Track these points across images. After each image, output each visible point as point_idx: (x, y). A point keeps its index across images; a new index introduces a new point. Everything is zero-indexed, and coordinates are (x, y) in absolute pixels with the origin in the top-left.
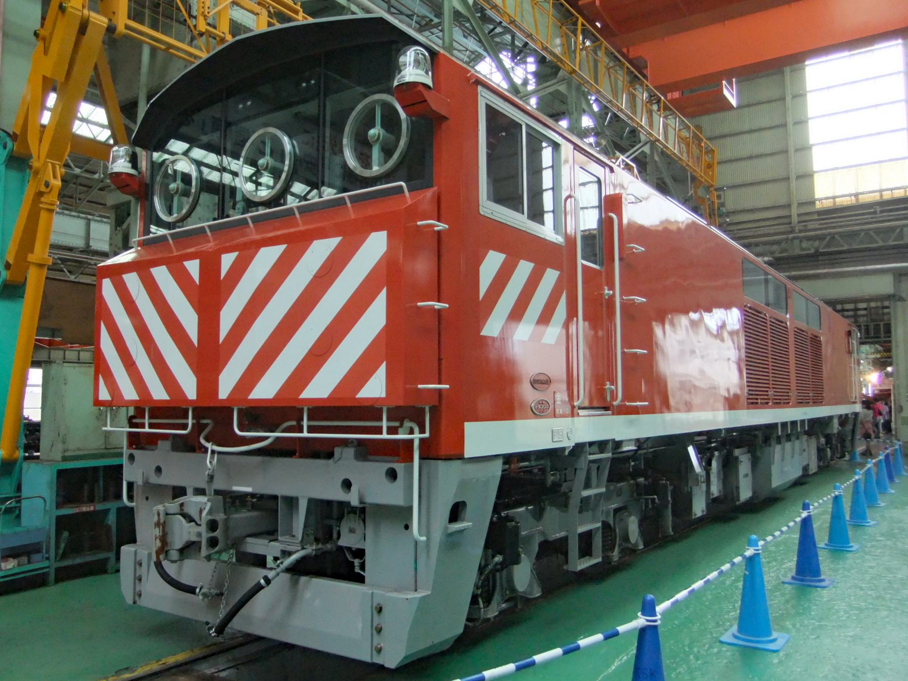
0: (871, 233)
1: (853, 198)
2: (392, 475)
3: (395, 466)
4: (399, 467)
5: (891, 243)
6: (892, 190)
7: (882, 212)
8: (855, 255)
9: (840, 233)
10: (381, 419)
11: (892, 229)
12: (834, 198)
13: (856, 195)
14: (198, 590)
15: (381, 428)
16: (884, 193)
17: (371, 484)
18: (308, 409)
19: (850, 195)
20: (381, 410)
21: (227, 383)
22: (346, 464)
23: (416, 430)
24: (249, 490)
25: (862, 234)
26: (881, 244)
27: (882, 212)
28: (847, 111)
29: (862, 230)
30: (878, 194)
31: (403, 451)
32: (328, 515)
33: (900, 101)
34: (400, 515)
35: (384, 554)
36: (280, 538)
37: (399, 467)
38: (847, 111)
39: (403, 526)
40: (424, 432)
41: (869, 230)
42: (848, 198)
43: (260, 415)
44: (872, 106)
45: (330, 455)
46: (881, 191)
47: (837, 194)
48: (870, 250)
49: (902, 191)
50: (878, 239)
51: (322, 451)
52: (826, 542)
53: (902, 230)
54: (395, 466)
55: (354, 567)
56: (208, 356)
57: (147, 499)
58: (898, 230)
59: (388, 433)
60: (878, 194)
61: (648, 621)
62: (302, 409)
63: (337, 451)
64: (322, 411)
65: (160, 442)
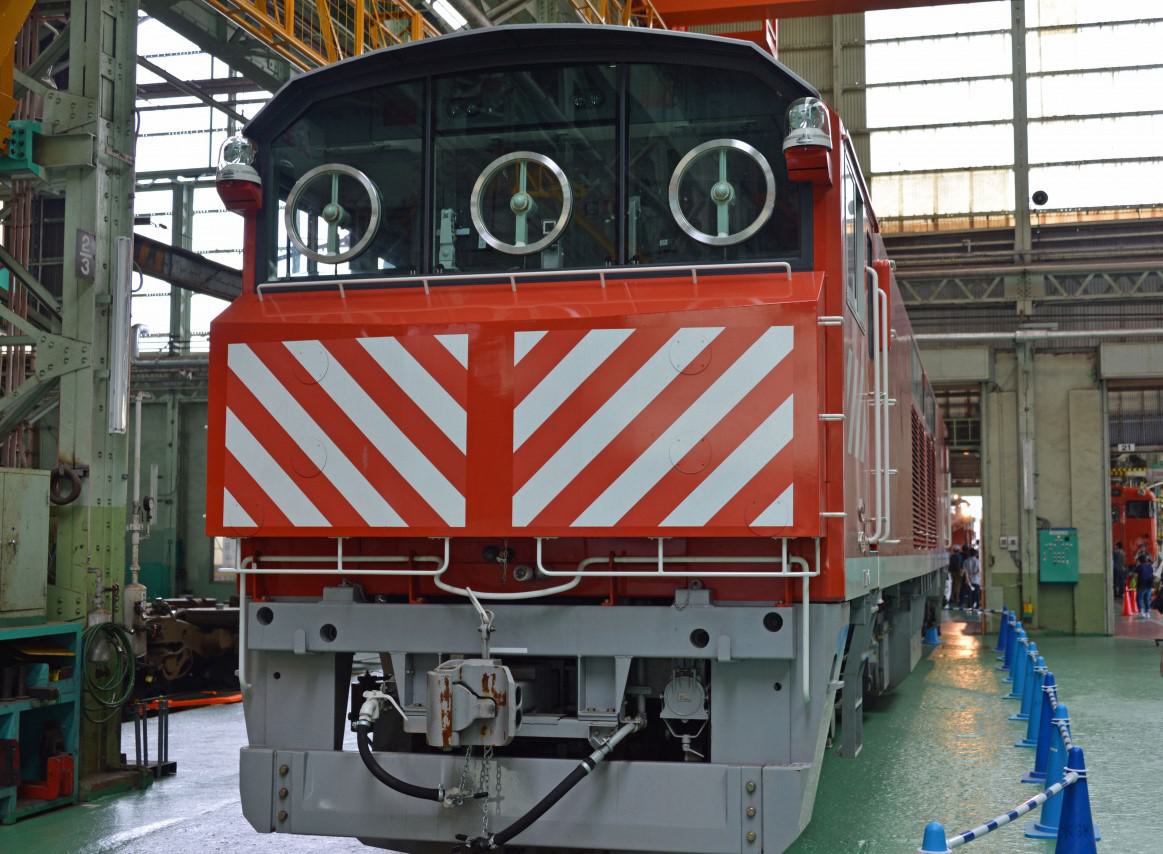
0: (957, 281)
1: (930, 221)
2: (773, 623)
3: (779, 611)
4: (786, 613)
5: (985, 299)
6: (988, 215)
7: (974, 249)
8: (929, 314)
9: (911, 277)
10: (335, 554)
11: (988, 278)
12: (901, 219)
13: (935, 218)
14: (441, 794)
15: (656, 564)
16: (976, 218)
17: (738, 634)
18: (344, 540)
19: (925, 217)
20: (780, 542)
21: (527, 506)
22: (693, 609)
23: (806, 566)
24: (523, 651)
25: (945, 281)
26: (971, 299)
27: (974, 249)
28: (925, 82)
29: (944, 276)
30: (966, 220)
31: (789, 592)
32: (649, 674)
33: (1004, 77)
34: (778, 673)
35: (740, 723)
36: (579, 713)
37: (786, 613)
38: (925, 82)
39: (773, 684)
40: (814, 570)
41: (955, 276)
42: (922, 222)
43: (571, 548)
44: (963, 79)
45: (667, 601)
46: (971, 215)
47: (905, 214)
48: (952, 307)
49: (1003, 217)
50: (968, 294)
51: (660, 596)
52: (1019, 713)
53: (1002, 280)
54: (779, 611)
55: (682, 744)
56: (489, 467)
57: (277, 676)
58: (997, 279)
59: (665, 570)
60: (966, 220)
61: (1080, 774)
62: (336, 540)
63: (680, 596)
64: (690, 543)
65: (327, 591)
